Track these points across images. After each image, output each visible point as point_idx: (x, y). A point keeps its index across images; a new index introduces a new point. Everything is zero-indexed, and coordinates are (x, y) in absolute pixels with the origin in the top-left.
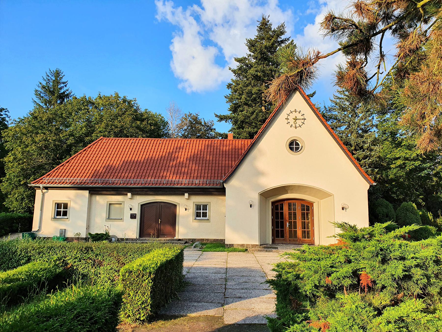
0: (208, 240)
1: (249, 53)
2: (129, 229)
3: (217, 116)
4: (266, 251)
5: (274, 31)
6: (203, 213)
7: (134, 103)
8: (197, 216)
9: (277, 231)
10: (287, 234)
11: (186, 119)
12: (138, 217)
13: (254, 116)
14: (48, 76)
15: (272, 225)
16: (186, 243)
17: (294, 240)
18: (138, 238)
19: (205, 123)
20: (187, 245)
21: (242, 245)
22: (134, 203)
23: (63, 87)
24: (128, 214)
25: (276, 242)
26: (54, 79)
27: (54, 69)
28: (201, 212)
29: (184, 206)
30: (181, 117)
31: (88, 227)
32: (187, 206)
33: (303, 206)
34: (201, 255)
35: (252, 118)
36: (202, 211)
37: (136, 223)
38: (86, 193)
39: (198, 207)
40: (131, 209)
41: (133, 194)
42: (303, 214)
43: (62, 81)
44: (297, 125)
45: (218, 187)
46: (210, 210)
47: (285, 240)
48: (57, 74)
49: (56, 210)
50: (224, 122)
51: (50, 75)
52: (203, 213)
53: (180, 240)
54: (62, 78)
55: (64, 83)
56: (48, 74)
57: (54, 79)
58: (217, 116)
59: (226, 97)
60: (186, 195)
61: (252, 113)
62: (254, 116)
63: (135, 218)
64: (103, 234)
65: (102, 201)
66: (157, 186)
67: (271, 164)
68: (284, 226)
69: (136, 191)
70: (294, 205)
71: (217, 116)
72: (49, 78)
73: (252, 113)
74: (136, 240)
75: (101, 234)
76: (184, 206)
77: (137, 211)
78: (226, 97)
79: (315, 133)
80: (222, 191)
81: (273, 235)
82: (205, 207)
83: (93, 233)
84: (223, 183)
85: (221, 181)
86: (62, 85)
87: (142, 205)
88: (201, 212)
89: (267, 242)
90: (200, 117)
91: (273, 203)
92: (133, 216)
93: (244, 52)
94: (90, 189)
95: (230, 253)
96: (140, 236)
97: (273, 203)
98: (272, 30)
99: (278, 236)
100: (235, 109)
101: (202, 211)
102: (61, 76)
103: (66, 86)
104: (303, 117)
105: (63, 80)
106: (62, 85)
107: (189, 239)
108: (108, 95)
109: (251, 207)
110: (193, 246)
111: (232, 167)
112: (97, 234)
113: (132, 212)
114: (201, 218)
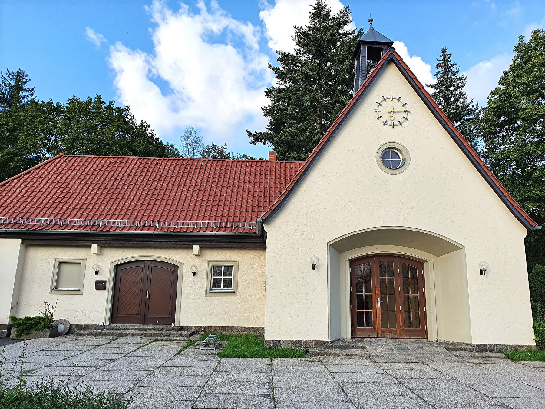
0: (232, 328)
1: (298, 47)
2: (92, 307)
3: (251, 134)
4: (346, 355)
5: (333, 18)
6: (225, 280)
7: (127, 114)
8: (215, 286)
9: (360, 314)
10: (378, 319)
11: (208, 153)
12: (110, 286)
13: (307, 134)
14: (4, 78)
15: (351, 304)
16: (193, 334)
17: (390, 331)
18: (107, 323)
19: (234, 158)
20: (194, 338)
21: (298, 343)
22: (101, 262)
23: (27, 96)
24: (90, 280)
25: (359, 334)
26: (13, 84)
27: (15, 70)
28: (221, 280)
29: (192, 266)
30: (201, 149)
31: (16, 305)
32: (196, 268)
33: (404, 268)
34: (216, 369)
35: (303, 137)
36: (222, 277)
37: (104, 299)
38: (14, 245)
39: (216, 270)
40: (97, 272)
41: (101, 247)
42: (406, 283)
43: (26, 87)
44: (396, 123)
45: (253, 233)
46: (236, 276)
47: (375, 331)
48: (19, 77)
49: (232, 277)
50: (260, 144)
51: (8, 78)
52: (225, 280)
53: (182, 328)
54: (25, 82)
55: (28, 90)
56: (5, 76)
57: (13, 84)
58: (250, 134)
59: (263, 109)
60: (196, 248)
61: (303, 131)
62: (307, 134)
63: (104, 288)
64: (40, 318)
65: (45, 258)
66: (143, 232)
67: (344, 192)
68: (373, 304)
69: (110, 240)
70: (390, 266)
71: (250, 134)
72: (6, 82)
73: (303, 131)
74: (103, 327)
75: (36, 318)
76: (192, 266)
77: (107, 276)
78: (263, 109)
79: (426, 138)
80: (258, 242)
81: (352, 322)
82: (229, 270)
83: (21, 316)
84: (262, 223)
85: (259, 220)
86: (27, 93)
87: (117, 266)
88: (221, 280)
89: (343, 336)
90: (227, 151)
91: (353, 262)
92: (100, 286)
93: (291, 47)
94: (23, 237)
95: (277, 362)
96: (112, 321)
97: (353, 262)
98: (331, 17)
99: (361, 324)
100: (276, 126)
101: (222, 277)
102: (24, 80)
103: (32, 95)
104: (404, 109)
105: (28, 86)
106: (27, 93)
107: (198, 327)
108: (84, 99)
109: (314, 268)
110: (203, 343)
111: (280, 193)
112: (28, 319)
113: (99, 278)
114: (222, 289)
